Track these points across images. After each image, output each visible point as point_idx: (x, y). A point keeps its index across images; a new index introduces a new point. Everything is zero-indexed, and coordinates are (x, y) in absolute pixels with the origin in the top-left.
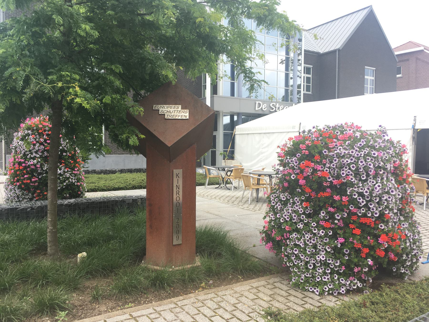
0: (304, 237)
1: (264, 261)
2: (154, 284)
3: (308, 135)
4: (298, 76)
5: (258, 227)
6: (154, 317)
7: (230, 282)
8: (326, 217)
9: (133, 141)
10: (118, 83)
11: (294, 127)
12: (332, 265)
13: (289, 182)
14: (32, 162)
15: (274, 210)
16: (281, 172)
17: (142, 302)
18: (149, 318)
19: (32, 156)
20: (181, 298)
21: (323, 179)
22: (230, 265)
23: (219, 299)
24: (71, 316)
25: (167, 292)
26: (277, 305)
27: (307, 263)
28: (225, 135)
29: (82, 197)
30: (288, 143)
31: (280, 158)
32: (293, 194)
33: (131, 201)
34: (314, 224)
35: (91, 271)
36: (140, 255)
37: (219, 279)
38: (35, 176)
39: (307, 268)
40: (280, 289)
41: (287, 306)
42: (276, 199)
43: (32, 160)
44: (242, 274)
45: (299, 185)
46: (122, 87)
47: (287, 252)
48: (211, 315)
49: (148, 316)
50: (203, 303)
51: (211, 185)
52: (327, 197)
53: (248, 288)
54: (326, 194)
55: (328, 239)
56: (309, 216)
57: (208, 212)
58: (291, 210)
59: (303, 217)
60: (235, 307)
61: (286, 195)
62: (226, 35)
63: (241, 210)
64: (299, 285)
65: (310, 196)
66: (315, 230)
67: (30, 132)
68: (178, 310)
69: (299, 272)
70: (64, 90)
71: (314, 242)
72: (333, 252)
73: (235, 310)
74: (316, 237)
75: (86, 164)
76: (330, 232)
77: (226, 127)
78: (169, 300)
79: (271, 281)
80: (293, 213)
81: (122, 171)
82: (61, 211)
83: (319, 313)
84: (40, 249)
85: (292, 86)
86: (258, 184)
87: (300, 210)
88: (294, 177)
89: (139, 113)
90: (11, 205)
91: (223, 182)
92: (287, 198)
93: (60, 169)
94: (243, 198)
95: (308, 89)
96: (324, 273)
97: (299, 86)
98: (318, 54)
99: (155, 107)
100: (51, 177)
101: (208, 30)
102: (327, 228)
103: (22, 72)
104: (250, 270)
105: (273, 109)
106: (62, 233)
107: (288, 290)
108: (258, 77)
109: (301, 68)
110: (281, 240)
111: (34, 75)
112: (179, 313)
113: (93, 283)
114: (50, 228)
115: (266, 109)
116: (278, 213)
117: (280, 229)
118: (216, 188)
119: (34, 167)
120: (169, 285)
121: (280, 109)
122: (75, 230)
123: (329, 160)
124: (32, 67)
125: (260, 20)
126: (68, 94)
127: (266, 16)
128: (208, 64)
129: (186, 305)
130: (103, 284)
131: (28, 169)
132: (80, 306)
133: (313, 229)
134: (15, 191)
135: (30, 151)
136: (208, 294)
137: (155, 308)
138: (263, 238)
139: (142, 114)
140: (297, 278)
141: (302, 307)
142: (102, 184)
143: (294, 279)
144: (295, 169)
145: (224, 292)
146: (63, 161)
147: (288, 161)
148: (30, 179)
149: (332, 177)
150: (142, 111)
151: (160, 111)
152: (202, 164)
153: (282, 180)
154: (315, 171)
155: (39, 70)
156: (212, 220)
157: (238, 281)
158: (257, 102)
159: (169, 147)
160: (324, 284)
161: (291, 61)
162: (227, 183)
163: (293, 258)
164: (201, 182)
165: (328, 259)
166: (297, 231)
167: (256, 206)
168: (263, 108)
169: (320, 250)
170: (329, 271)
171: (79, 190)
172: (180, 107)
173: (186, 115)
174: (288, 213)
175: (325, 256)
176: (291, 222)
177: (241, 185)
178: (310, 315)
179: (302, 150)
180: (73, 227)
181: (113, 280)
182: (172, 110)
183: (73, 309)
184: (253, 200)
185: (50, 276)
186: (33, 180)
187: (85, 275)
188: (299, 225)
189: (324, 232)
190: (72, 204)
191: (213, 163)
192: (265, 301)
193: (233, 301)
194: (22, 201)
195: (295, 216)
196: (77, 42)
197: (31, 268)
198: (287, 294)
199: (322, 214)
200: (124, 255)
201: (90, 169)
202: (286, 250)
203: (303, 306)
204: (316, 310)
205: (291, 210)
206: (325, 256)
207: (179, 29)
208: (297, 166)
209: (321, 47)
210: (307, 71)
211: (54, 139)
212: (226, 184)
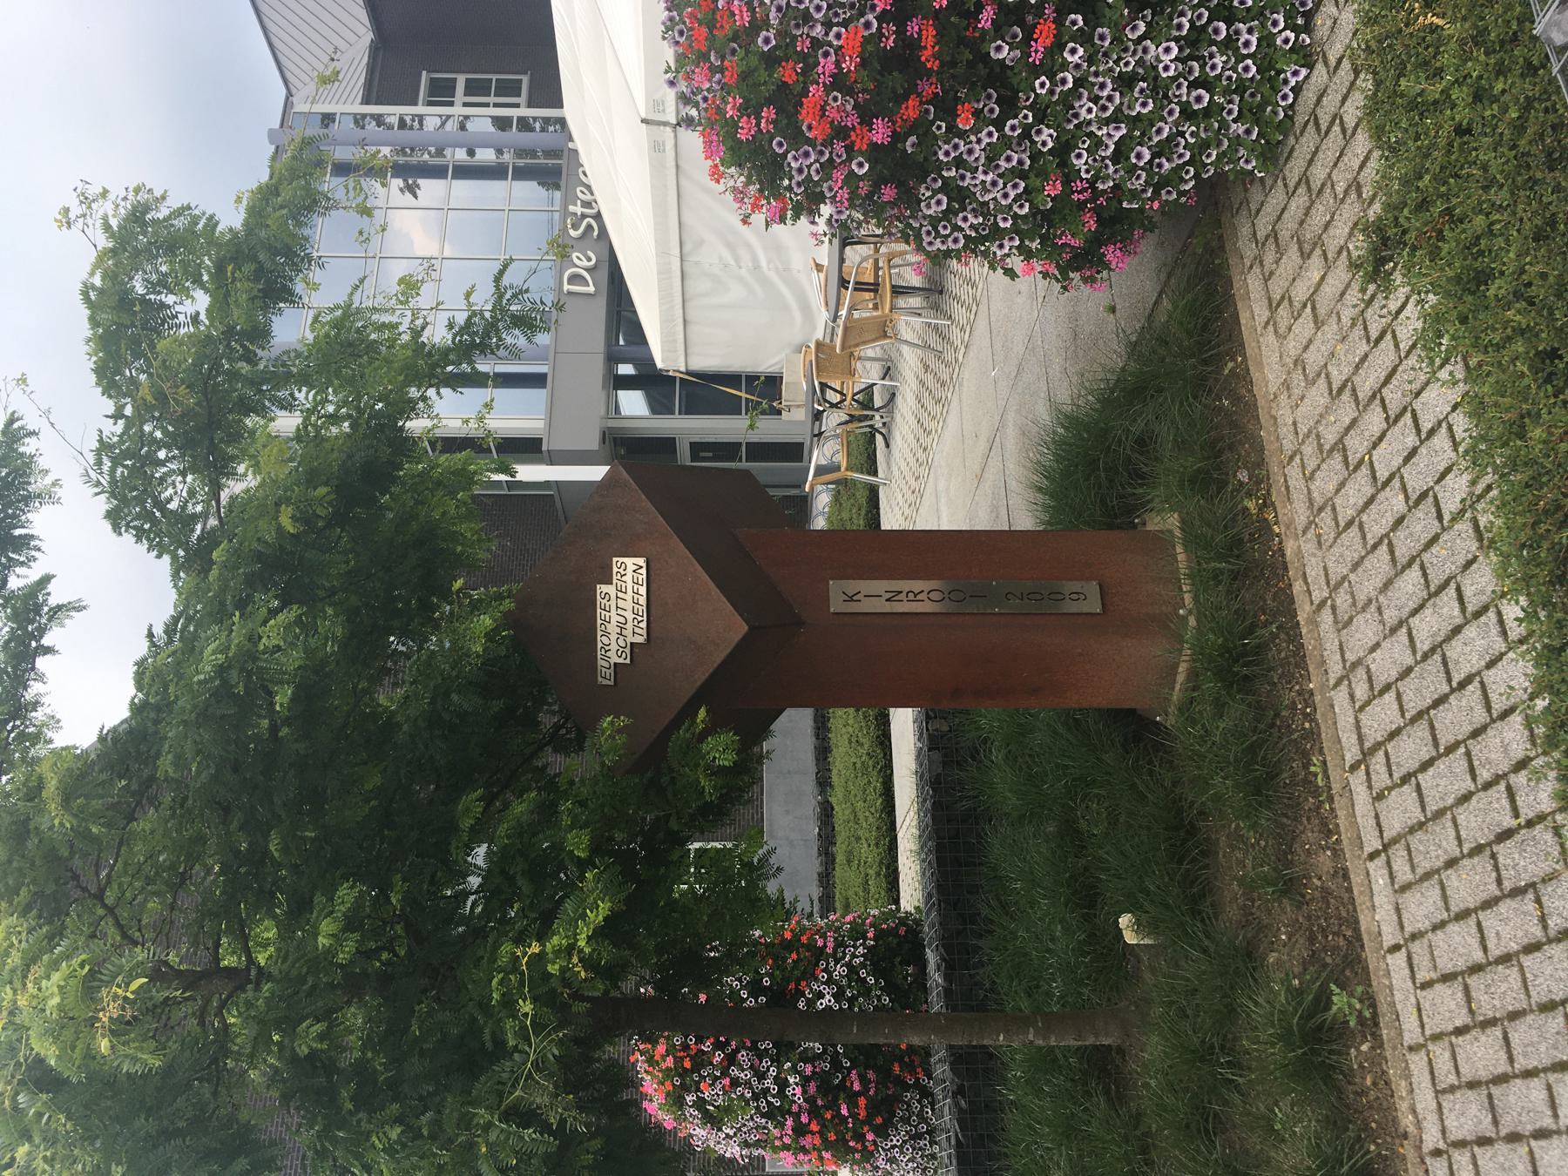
0: (1089, 123)
1: (1169, 276)
2: (1245, 684)
3: (703, 105)
4: (463, 127)
5: (1041, 294)
6: (1366, 686)
7: (1251, 408)
8: (1015, 36)
9: (720, 750)
10: (520, 809)
11: (657, 147)
12: (1200, 16)
13: (877, 181)
14: (795, 1091)
15: (982, 239)
16: (839, 212)
17: (1307, 725)
18: (1368, 703)
19: (775, 1089)
20: (1298, 587)
21: (869, 48)
22: (1181, 404)
23: (1309, 449)
24: (1348, 973)
25: (1274, 636)
26: (1340, 231)
27: (1187, 114)
28: (690, 408)
29: (918, 922)
30: (731, 183)
31: (789, 213)
32: (924, 167)
33: (937, 755)
34: (1042, 85)
35: (1187, 900)
36: (1134, 728)
37: (1231, 447)
38: (844, 1079)
39: (1207, 113)
40: (1279, 218)
41: (1346, 192)
42: (943, 232)
43: (789, 1092)
44: (1219, 360)
45: (893, 144)
46: (533, 794)
47: (1144, 191)
48: (1370, 480)
49: (1362, 709)
50: (1321, 509)
51: (875, 462)
52: (940, 36)
53: (1271, 338)
54: (929, 37)
55: (1100, 30)
56: (1009, 106)
57: (980, 478)
58: (985, 173)
59: (1013, 128)
60: (1341, 390)
61: (928, 194)
62: (334, 419)
63: (971, 354)
64: (1267, 142)
65: (935, 100)
66: (1064, 81)
67: (689, 1099)
68: (1342, 599)
69: (1219, 144)
70: (553, 991)
71: (1110, 86)
72: (1148, 12)
73: (1354, 390)
74: (1092, 79)
75: (799, 907)
76: (1074, 23)
77: (659, 406)
78: (1304, 631)
79: (1249, 251)
80: (998, 166)
81: (824, 783)
82: (969, 998)
83: (1382, 75)
84: (1103, 1069)
85: (499, 152)
86: (874, 287)
87: (986, 140)
88: (861, 165)
89: (619, 731)
90: (946, 1161)
91: (867, 418)
92: (940, 190)
93: (821, 995)
94: (926, 347)
95: (510, 89)
96: (1227, 48)
97: (502, 124)
98: (375, 50)
99: (605, 677)
100: (855, 1034)
101: (322, 491)
102: (1058, 36)
103: (493, 1136)
104: (1204, 328)
105: (589, 227)
106: (1049, 994)
107: (1286, 185)
108: (484, 299)
109: (432, 116)
110: (1098, 211)
111: (500, 1095)
112: (1353, 597)
113: (1231, 894)
114: (1031, 1037)
115: (590, 254)
116: (995, 223)
117: (1056, 218)
118: (888, 446)
119: (812, 1084)
120: (1250, 631)
121: (588, 197)
122: (1036, 949)
123: (797, 26)
124: (473, 1104)
125: (277, 292)
126: (566, 976)
127: (260, 272)
128: (439, 483)
129: (1325, 569)
130: (1238, 859)
131: (820, 1102)
132: (1312, 939)
133: (1058, 90)
134: (893, 1147)
135: (756, 1097)
136: (1287, 488)
137: (1332, 682)
138: (1085, 280)
139: (623, 721)
140: (1242, 152)
141: (1353, 134)
142: (868, 853)
143: (1247, 162)
144: (831, 160)
145: (1283, 431)
146: (792, 986)
147: (799, 185)
148: (852, 1098)
149: (862, 14)
150: (612, 723)
151: (621, 661)
152: (793, 492)
153: (873, 208)
154: (838, 82)
155: (483, 1079)
156: (1011, 465)
157: (1243, 376)
158: (566, 287)
159: (751, 628)
160: (1269, 46)
161: (405, 154)
162: (867, 404)
163: (1167, 166)
164: (864, 501)
165: (1175, 33)
166: (1064, 148)
167: (956, 298)
168: (586, 263)
169: (1140, 63)
170: (1222, 26)
171: (893, 932)
172: (602, 588)
173: (631, 568)
174: (994, 183)
175: (1164, 45)
176: (1031, 175)
177: (878, 352)
178: (1387, 107)
179: (760, 130)
180: (1025, 955)
181: (1223, 826)
182: (615, 618)
183: (1325, 965)
184: (936, 308)
185: (1203, 1042)
186: (857, 1087)
187: (1203, 921)
188: (1044, 144)
189: (1071, 45)
190: (943, 959)
191: (793, 452)
192: (1323, 278)
193: (1318, 396)
194: (928, 1124)
195: (1008, 159)
196: (379, 949)
197: (1169, 1100)
198: (1302, 190)
199: (1004, 53)
200: (1134, 786)
201: (816, 892)
202: (1134, 195)
203: (1349, 132)
204: (1366, 82)
205: (985, 173)
206: (1164, 45)
207: (321, 593)
208: (821, 153)
209: (352, 38)
210: (441, 93)
211: (725, 1022)
212: (872, 409)
